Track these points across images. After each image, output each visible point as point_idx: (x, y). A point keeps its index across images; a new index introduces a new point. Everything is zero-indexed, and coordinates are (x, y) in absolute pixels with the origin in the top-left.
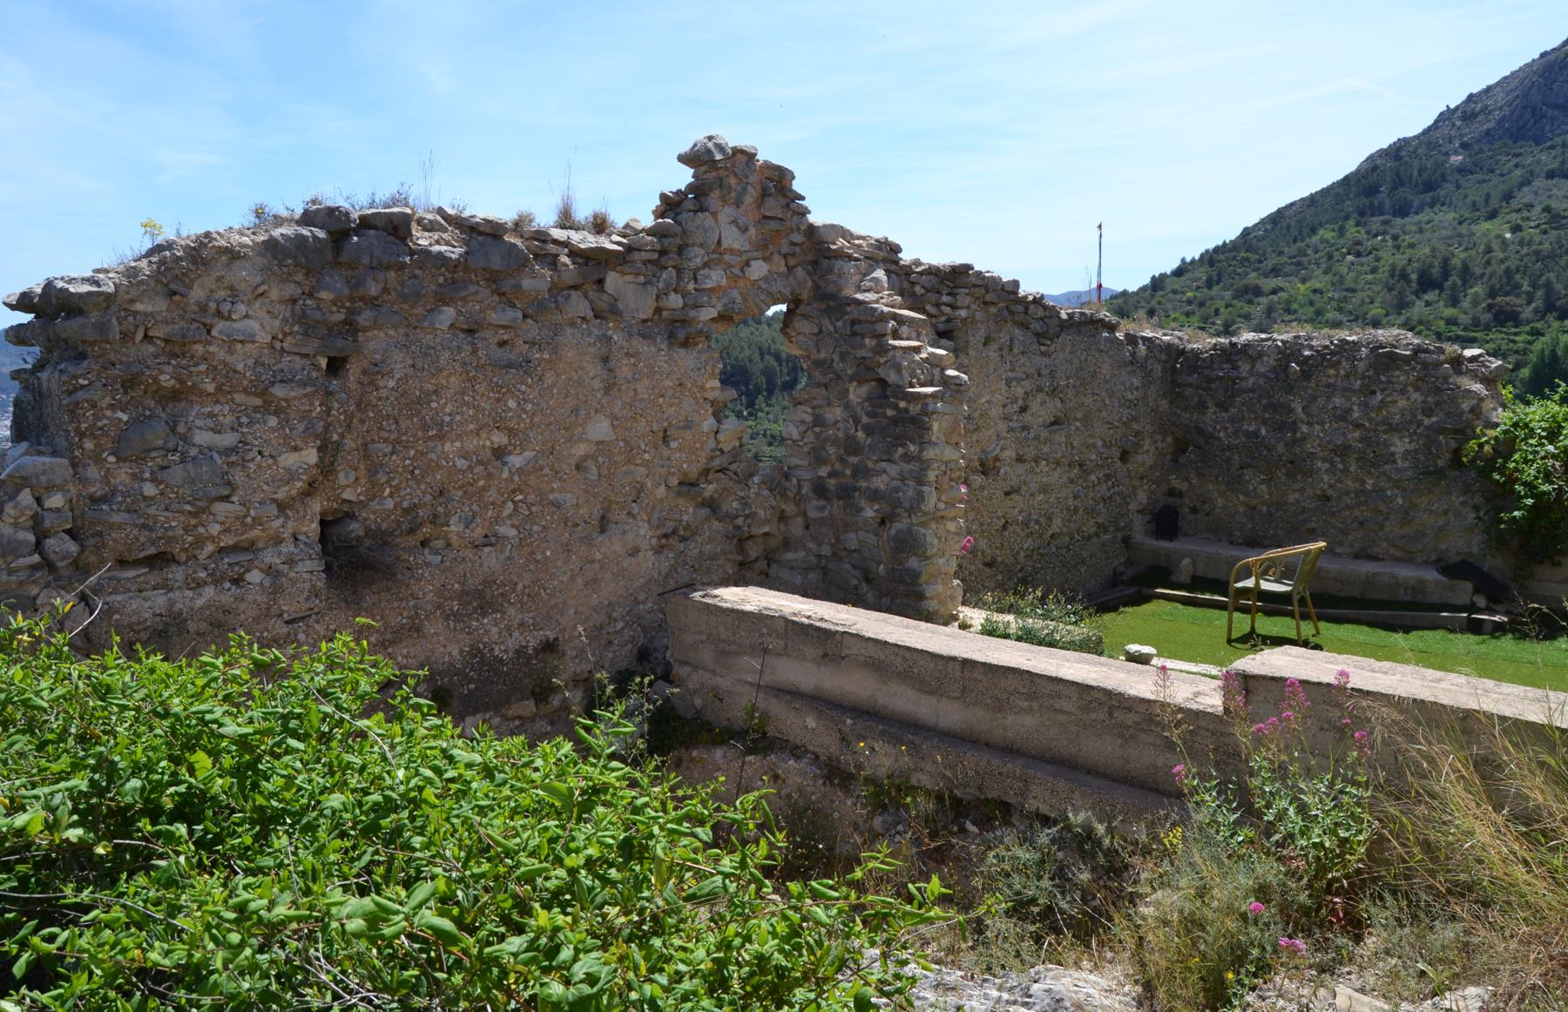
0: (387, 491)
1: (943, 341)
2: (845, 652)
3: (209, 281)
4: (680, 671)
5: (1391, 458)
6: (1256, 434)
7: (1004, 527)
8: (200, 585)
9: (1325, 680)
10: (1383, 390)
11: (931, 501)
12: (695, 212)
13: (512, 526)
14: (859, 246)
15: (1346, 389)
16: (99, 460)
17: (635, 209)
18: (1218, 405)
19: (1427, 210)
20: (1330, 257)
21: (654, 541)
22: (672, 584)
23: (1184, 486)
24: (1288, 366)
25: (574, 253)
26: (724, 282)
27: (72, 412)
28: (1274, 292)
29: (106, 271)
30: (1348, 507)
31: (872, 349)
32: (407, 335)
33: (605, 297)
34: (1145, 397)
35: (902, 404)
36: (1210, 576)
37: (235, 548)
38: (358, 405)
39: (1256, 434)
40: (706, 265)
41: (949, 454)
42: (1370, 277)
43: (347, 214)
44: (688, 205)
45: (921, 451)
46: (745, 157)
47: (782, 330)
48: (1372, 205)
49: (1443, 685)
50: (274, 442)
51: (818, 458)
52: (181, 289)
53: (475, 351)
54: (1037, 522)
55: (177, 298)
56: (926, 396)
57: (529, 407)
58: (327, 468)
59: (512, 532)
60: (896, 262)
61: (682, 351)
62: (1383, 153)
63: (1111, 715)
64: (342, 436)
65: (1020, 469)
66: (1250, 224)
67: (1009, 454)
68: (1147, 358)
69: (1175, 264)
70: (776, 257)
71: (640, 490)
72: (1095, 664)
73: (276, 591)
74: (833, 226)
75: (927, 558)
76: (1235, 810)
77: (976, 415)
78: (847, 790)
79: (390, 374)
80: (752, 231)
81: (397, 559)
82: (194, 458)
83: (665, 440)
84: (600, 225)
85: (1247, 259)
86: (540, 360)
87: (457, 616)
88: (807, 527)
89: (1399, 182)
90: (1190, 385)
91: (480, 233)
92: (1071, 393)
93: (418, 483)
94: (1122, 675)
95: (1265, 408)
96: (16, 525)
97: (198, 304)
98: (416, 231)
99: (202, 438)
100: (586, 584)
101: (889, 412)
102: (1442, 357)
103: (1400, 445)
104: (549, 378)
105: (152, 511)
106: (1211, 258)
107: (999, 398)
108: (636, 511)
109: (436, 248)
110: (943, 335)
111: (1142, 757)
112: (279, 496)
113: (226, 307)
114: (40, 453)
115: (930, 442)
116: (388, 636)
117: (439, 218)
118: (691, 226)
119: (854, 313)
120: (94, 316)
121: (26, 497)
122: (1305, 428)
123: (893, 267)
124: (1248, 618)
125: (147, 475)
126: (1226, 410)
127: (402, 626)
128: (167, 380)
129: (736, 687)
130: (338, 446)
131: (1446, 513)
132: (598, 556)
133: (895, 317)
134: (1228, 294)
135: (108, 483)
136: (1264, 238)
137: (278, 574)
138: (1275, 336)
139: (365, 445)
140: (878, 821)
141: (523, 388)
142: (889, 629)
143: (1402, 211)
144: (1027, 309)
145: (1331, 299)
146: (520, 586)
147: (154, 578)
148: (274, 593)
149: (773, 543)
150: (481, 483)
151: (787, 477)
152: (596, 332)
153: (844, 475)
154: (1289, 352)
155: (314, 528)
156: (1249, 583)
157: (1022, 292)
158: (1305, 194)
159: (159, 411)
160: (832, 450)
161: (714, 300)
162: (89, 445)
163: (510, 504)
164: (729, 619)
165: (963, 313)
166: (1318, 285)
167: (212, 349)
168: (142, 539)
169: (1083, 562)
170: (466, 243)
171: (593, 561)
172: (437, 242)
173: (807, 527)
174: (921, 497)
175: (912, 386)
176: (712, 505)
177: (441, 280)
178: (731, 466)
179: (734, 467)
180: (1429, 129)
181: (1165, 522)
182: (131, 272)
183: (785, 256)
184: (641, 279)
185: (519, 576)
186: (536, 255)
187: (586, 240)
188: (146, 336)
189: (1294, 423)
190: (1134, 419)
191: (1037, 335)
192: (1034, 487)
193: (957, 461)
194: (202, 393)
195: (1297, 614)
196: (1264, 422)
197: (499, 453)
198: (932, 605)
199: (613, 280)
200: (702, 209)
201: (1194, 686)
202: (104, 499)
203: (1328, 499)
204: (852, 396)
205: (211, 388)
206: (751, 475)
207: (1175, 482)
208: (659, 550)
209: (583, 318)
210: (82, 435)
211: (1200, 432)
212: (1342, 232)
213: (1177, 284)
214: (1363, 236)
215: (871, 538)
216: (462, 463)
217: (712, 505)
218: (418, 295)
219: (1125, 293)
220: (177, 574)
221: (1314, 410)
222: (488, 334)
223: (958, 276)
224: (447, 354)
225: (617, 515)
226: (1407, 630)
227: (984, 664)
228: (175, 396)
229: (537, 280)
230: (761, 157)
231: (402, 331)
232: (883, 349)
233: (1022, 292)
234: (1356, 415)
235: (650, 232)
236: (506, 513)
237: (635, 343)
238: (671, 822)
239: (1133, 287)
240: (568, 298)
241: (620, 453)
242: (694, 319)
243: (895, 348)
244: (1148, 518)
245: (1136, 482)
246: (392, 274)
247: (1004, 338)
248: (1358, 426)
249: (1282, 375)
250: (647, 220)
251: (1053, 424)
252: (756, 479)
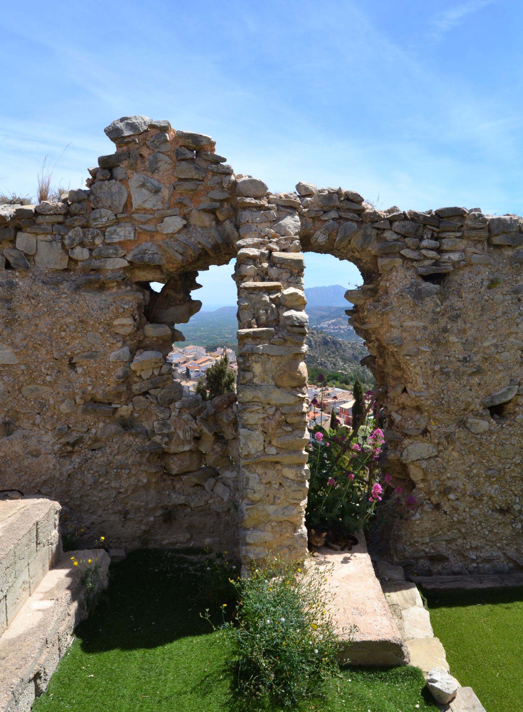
12: (104, 180)
165: (455, 257)
217: (127, 425)
252: (177, 404)
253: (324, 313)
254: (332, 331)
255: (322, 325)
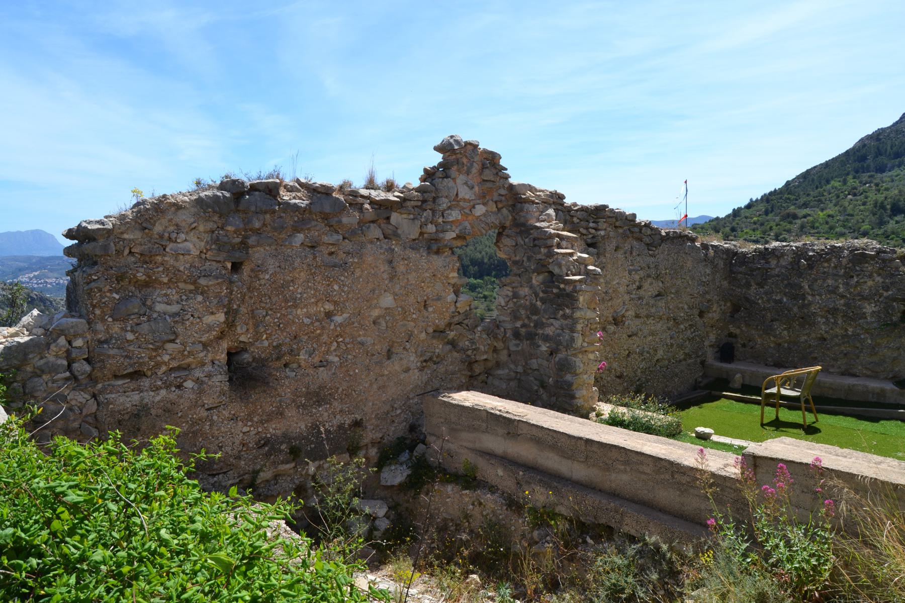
0: (265, 336)
1: (591, 249)
2: (520, 432)
3: (164, 221)
4: (430, 439)
5: (863, 316)
6: (780, 301)
7: (628, 355)
8: (158, 389)
9: (805, 461)
10: (858, 276)
11: (579, 342)
13: (336, 355)
14: (539, 196)
15: (835, 275)
16: (103, 320)
17: (410, 177)
18: (758, 284)
19: (896, 169)
20: (838, 197)
21: (419, 364)
22: (429, 388)
23: (738, 331)
24: (799, 261)
25: (373, 202)
26: (460, 217)
27: (89, 294)
28: (805, 217)
29: (111, 217)
30: (836, 344)
31: (545, 254)
32: (276, 249)
33: (390, 227)
34: (714, 280)
35: (562, 286)
36: (753, 384)
37: (179, 368)
38: (248, 289)
39: (780, 301)
40: (449, 208)
41: (590, 314)
42: (862, 207)
43: (243, 183)
44: (439, 174)
45: (573, 313)
46: (473, 147)
47: (495, 244)
48: (863, 167)
49: (883, 466)
50: (201, 310)
51: (515, 317)
52: (149, 226)
53: (315, 258)
54: (648, 352)
55: (147, 231)
56: (575, 281)
57: (346, 289)
58: (230, 324)
59: (336, 359)
60: (562, 205)
61: (435, 257)
62: (869, 137)
63: (673, 476)
64: (239, 306)
65: (638, 322)
66: (790, 179)
67: (631, 313)
68: (714, 257)
69: (747, 202)
70: (491, 202)
71: (410, 336)
72: (665, 444)
73: (201, 392)
74: (524, 185)
75: (577, 375)
76: (747, 541)
77: (610, 291)
78: (520, 515)
79: (266, 271)
80: (476, 189)
81: (270, 374)
82: (155, 319)
83: (425, 306)
84: (390, 187)
85: (789, 199)
86: (352, 263)
87: (304, 406)
88: (510, 356)
89: (879, 153)
90: (741, 273)
91: (319, 193)
92: (668, 278)
93: (282, 331)
94: (681, 452)
95: (786, 286)
96: (57, 356)
97: (158, 234)
98: (282, 192)
99: (160, 307)
100: (379, 388)
101: (555, 291)
102: (895, 256)
103: (869, 308)
104: (358, 273)
105: (131, 348)
106: (767, 198)
107: (625, 281)
108: (408, 347)
109: (294, 201)
110: (591, 245)
111: (691, 504)
112: (203, 339)
113: (174, 236)
114: (73, 316)
115: (578, 308)
116: (265, 417)
117: (296, 185)
118: (440, 186)
119: (535, 234)
120: (101, 242)
121: (62, 341)
122: (810, 298)
123: (560, 207)
124: (773, 410)
125: (129, 328)
126: (763, 287)
127: (273, 412)
128: (141, 276)
129: (458, 449)
130: (236, 312)
131: (898, 349)
132: (386, 372)
133: (558, 236)
134: (778, 219)
135: (108, 333)
136: (798, 186)
137: (202, 383)
138: (792, 244)
139: (253, 311)
140: (536, 534)
141: (343, 278)
142: (546, 418)
143: (881, 169)
144: (641, 230)
145: (838, 220)
146: (341, 389)
147: (133, 385)
148: (200, 393)
149: (490, 364)
150: (318, 332)
151: (498, 327)
152: (385, 246)
153: (530, 327)
154: (800, 253)
155: (223, 357)
156: (774, 390)
157: (638, 220)
158: (823, 161)
159: (137, 293)
160: (523, 312)
161: (454, 228)
162: (98, 312)
163: (335, 344)
164: (456, 410)
165: (602, 233)
166: (831, 213)
167: (166, 259)
168: (126, 364)
169: (677, 375)
170: (310, 198)
171: (383, 376)
172: (294, 198)
173: (510, 356)
174: (572, 339)
175: (568, 275)
176: (453, 344)
177: (296, 219)
178: (465, 320)
179: (466, 322)
180: (897, 123)
181: (726, 352)
182: (122, 217)
183: (496, 202)
184: (412, 216)
185: (340, 384)
186: (351, 204)
187: (379, 195)
188: (130, 252)
189: (803, 294)
190: (707, 293)
191: (648, 245)
192: (646, 332)
193: (594, 319)
194: (161, 283)
195: (803, 408)
196: (785, 294)
197: (329, 315)
198: (579, 402)
199: (395, 217)
200: (447, 177)
201: (721, 463)
202: (106, 342)
203: (825, 339)
204: (534, 281)
205: (165, 280)
206: (476, 326)
207: (732, 329)
208: (421, 369)
209: (378, 239)
210: (94, 306)
211: (747, 300)
212: (845, 182)
213: (748, 213)
214: (857, 184)
215: (545, 363)
216: (307, 321)
217: (453, 344)
218: (282, 227)
219: (717, 218)
220: (146, 383)
221: (815, 287)
222: (322, 248)
223: (599, 212)
224: (299, 260)
225: (397, 349)
226: (875, 419)
227: (599, 442)
228: (147, 284)
229: (351, 219)
230: (482, 147)
231: (274, 247)
232: (551, 254)
233: (638, 220)
234: (841, 290)
235: (417, 190)
236: (333, 348)
237: (407, 252)
238: (284, 587)
239: (722, 215)
240: (369, 227)
241: (399, 314)
242: (442, 238)
243: (558, 253)
244: (716, 350)
245: (708, 329)
246: (268, 216)
247: (627, 246)
248: (842, 297)
249: (796, 267)
250: (416, 183)
251: (657, 296)
252: (479, 329)
253: (22, 264)
254: (36, 286)
255: (20, 278)
